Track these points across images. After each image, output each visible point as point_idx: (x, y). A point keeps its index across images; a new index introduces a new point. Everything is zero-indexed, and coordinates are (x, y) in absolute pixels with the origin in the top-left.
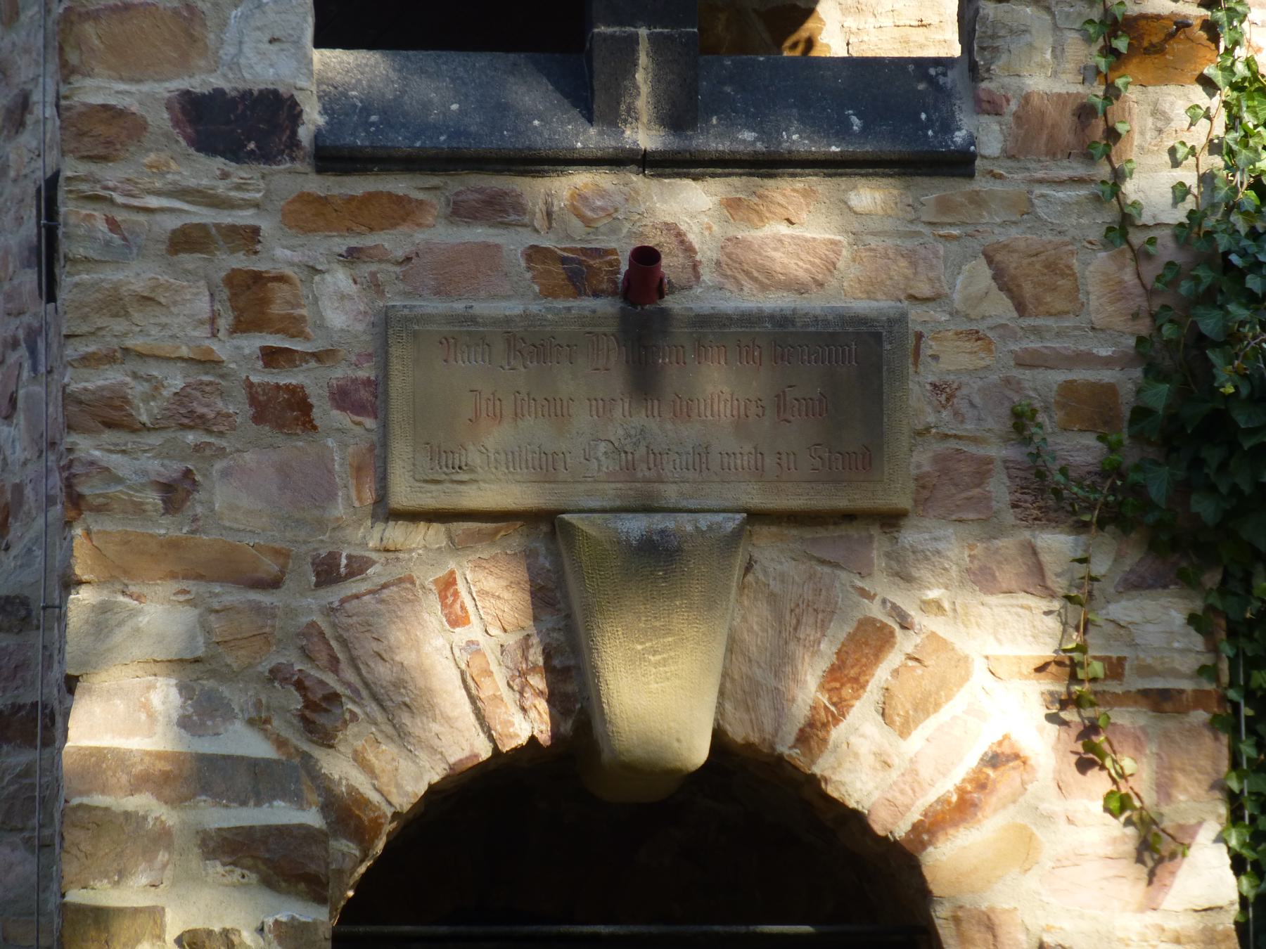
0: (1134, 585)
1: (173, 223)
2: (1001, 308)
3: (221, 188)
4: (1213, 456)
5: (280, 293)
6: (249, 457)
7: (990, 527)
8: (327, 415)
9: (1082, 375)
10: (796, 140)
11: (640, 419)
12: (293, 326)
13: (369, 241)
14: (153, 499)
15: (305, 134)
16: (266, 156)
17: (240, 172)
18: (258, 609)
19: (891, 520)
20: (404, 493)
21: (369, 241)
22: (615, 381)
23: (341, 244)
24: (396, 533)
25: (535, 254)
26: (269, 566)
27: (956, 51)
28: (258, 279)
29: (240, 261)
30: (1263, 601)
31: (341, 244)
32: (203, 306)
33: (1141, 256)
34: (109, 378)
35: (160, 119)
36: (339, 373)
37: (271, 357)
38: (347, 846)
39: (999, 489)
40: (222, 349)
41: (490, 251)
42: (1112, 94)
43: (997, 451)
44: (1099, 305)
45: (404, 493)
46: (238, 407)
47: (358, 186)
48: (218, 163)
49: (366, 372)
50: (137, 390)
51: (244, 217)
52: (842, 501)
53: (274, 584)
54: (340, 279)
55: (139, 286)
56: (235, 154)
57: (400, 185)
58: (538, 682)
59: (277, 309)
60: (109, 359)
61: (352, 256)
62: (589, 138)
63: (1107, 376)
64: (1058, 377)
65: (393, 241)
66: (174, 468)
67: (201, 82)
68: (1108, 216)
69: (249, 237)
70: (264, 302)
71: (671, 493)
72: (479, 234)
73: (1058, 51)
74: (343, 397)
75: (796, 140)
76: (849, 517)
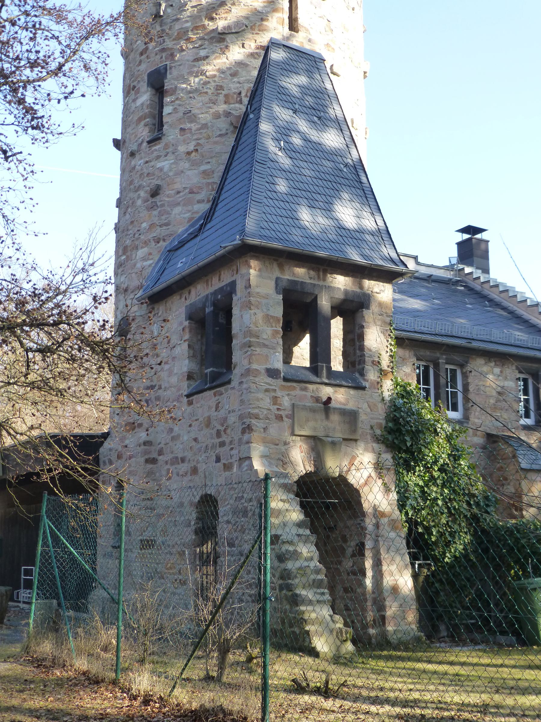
0: (387, 452)
1: (265, 388)
2: (369, 410)
3: (271, 383)
4: (398, 434)
5: (279, 399)
6: (275, 425)
7: (367, 443)
8: (285, 419)
9: (378, 421)
10: (344, 383)
11: (327, 423)
12: (280, 405)
13: (290, 393)
14: (262, 430)
15: (282, 375)
16: (277, 378)
17: (274, 381)
18: (277, 449)
19: (356, 440)
20: (297, 432)
21: (290, 393)
22: (323, 417)
23: (287, 393)
24: (294, 438)
25: (312, 396)
26: (277, 442)
27: (307, 364)
28: (276, 397)
29: (274, 394)
30: (538, 508)
31: (287, 393)
32: (269, 401)
33: (385, 404)
34: (256, 411)
35: (263, 371)
36: (287, 413)
37: (278, 409)
38: (530, 674)
39: (369, 437)
40: (271, 407)
41: (306, 395)
42: (381, 380)
43: (369, 431)
44: (380, 410)
45: (297, 432)
46: (274, 417)
47: (289, 384)
48: (271, 379)
49: (290, 413)
50: (260, 413)
51: (273, 387)
52: (351, 437)
53: (277, 445)
54: (286, 398)
55: (261, 397)
56: (272, 377)
57: (294, 384)
58: (312, 462)
59: (278, 402)
60: (256, 408)
61: (288, 395)
62: (318, 380)
63: (381, 421)
64: (376, 421)
65: (293, 393)
66: (264, 426)
67: (269, 366)
68: (381, 398)
69: (275, 391)
70: (277, 401)
71: (331, 435)
72: (304, 393)
73: (374, 373)
74: (287, 416)
75: (344, 383)
76: (351, 440)
